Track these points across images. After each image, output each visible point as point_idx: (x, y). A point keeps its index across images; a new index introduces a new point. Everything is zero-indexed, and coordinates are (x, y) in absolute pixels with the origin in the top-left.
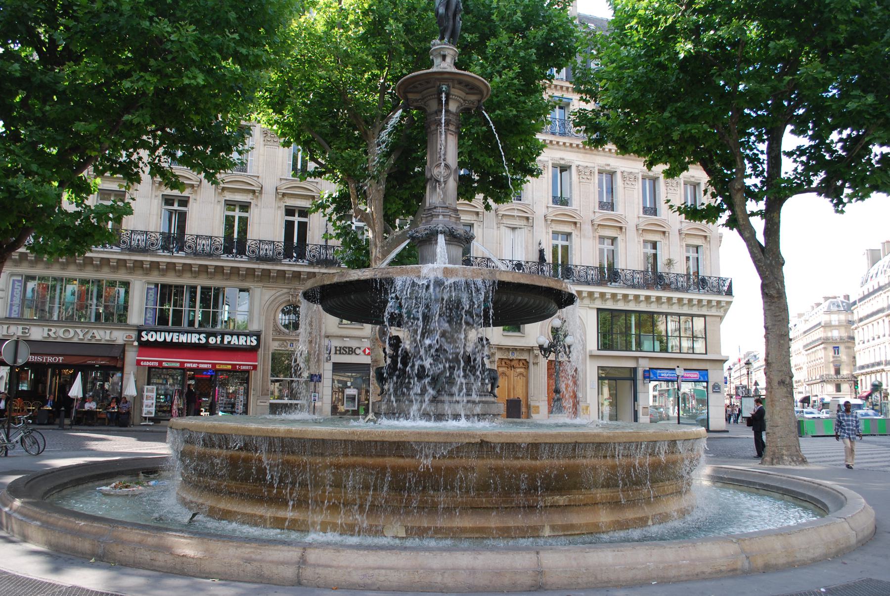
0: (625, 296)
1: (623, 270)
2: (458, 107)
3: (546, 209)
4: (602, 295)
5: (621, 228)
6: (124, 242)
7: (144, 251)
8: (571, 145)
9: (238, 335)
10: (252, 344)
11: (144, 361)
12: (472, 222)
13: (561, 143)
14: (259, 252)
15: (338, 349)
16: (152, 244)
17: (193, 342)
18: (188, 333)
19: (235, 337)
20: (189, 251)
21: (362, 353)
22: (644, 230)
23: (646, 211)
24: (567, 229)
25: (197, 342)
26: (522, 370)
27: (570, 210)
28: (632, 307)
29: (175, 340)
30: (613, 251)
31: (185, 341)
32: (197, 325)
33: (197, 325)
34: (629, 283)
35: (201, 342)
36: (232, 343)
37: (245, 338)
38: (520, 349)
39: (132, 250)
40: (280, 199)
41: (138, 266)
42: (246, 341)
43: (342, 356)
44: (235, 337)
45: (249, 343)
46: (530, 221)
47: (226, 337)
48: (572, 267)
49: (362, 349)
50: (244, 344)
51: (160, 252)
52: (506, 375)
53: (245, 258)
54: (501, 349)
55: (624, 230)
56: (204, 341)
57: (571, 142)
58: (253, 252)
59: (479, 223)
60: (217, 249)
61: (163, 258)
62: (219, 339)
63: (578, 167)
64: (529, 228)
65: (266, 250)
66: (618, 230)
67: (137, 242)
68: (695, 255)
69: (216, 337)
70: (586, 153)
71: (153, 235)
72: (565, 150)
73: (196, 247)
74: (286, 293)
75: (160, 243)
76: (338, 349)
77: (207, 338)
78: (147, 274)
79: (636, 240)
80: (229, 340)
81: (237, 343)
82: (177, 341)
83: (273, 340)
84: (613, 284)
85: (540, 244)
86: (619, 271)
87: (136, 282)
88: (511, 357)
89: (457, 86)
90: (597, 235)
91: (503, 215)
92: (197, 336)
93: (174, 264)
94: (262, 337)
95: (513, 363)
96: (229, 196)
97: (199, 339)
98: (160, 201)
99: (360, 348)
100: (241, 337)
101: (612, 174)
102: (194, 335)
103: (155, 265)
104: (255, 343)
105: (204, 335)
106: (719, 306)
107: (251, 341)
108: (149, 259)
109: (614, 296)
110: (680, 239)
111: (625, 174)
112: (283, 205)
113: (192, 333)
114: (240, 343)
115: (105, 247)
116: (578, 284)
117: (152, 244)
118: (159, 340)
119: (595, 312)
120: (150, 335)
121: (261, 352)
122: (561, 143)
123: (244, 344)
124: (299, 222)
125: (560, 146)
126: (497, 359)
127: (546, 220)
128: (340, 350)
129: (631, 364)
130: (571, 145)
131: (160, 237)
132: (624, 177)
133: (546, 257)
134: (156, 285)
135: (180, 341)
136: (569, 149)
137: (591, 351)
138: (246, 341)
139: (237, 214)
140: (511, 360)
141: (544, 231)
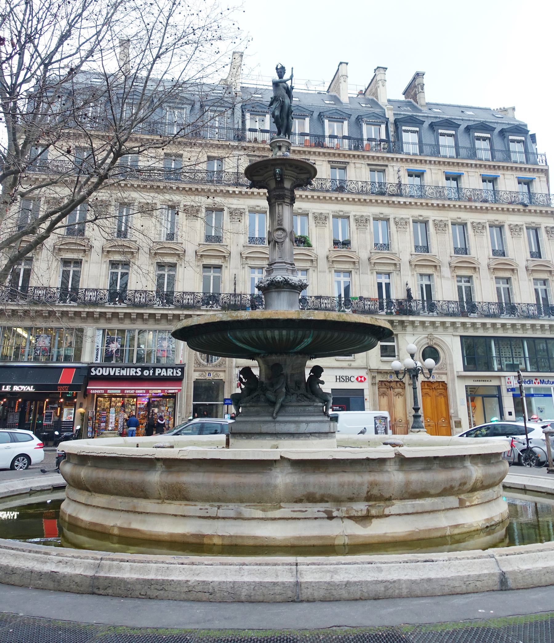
0: (484, 325)
2: (292, 184)
3: (410, 256)
4: (464, 324)
5: (475, 268)
6: (80, 298)
7: (95, 304)
10: (177, 375)
11: (93, 389)
12: (350, 270)
13: (457, 206)
14: (183, 301)
15: (338, 377)
16: (101, 299)
17: (131, 374)
18: (127, 367)
19: (164, 370)
20: (129, 303)
21: (356, 381)
22: (494, 269)
24: (507, 274)
25: (134, 374)
26: (400, 390)
27: (468, 258)
29: (117, 374)
30: (508, 288)
31: (125, 374)
32: (135, 361)
33: (135, 361)
34: (525, 314)
35: (137, 374)
36: (162, 375)
37: (172, 370)
38: (384, 372)
39: (85, 304)
40: (199, 260)
41: (90, 315)
42: (173, 373)
43: (341, 383)
44: (164, 370)
45: (175, 374)
46: (398, 266)
47: (157, 370)
48: (435, 302)
49: (356, 377)
50: (171, 375)
51: (107, 305)
52: (386, 395)
53: (172, 307)
54: (381, 373)
55: (477, 270)
56: (139, 374)
58: (178, 301)
59: (356, 270)
60: (199, 302)
61: (109, 309)
62: (151, 372)
64: (397, 272)
65: (91, 296)
67: (89, 298)
69: (149, 371)
70: (440, 210)
71: (102, 291)
72: (422, 209)
73: (134, 300)
74: (424, 338)
75: (107, 297)
76: (338, 377)
77: (142, 372)
78: (97, 322)
79: (489, 278)
80: (160, 372)
81: (165, 375)
82: (119, 374)
83: (195, 371)
84: (472, 314)
85: (407, 284)
86: (476, 304)
87: (89, 328)
88: (389, 379)
89: (289, 168)
90: (455, 275)
91: (375, 263)
92: (135, 370)
93: (118, 313)
94: (186, 369)
95: (392, 384)
96: (159, 259)
97: (136, 372)
98: (108, 265)
100: (169, 370)
102: (132, 369)
103: (102, 315)
104: (180, 374)
105: (140, 369)
106: (525, 328)
107: (177, 373)
108: (98, 310)
109: (503, 325)
110: (527, 274)
111: (474, 224)
112: (201, 264)
113: (130, 368)
114: (168, 375)
115: (116, 304)
116: (442, 316)
117: (101, 299)
118: (104, 374)
119: (459, 338)
120: (97, 371)
121: (185, 381)
122: (419, 204)
123: (171, 375)
124: (118, 273)
125: (418, 206)
126: (377, 382)
127: (411, 265)
129: (495, 383)
130: (503, 209)
131: (107, 293)
134: (104, 330)
135: (121, 374)
136: (425, 207)
138: (173, 373)
140: (391, 382)
141: (410, 273)
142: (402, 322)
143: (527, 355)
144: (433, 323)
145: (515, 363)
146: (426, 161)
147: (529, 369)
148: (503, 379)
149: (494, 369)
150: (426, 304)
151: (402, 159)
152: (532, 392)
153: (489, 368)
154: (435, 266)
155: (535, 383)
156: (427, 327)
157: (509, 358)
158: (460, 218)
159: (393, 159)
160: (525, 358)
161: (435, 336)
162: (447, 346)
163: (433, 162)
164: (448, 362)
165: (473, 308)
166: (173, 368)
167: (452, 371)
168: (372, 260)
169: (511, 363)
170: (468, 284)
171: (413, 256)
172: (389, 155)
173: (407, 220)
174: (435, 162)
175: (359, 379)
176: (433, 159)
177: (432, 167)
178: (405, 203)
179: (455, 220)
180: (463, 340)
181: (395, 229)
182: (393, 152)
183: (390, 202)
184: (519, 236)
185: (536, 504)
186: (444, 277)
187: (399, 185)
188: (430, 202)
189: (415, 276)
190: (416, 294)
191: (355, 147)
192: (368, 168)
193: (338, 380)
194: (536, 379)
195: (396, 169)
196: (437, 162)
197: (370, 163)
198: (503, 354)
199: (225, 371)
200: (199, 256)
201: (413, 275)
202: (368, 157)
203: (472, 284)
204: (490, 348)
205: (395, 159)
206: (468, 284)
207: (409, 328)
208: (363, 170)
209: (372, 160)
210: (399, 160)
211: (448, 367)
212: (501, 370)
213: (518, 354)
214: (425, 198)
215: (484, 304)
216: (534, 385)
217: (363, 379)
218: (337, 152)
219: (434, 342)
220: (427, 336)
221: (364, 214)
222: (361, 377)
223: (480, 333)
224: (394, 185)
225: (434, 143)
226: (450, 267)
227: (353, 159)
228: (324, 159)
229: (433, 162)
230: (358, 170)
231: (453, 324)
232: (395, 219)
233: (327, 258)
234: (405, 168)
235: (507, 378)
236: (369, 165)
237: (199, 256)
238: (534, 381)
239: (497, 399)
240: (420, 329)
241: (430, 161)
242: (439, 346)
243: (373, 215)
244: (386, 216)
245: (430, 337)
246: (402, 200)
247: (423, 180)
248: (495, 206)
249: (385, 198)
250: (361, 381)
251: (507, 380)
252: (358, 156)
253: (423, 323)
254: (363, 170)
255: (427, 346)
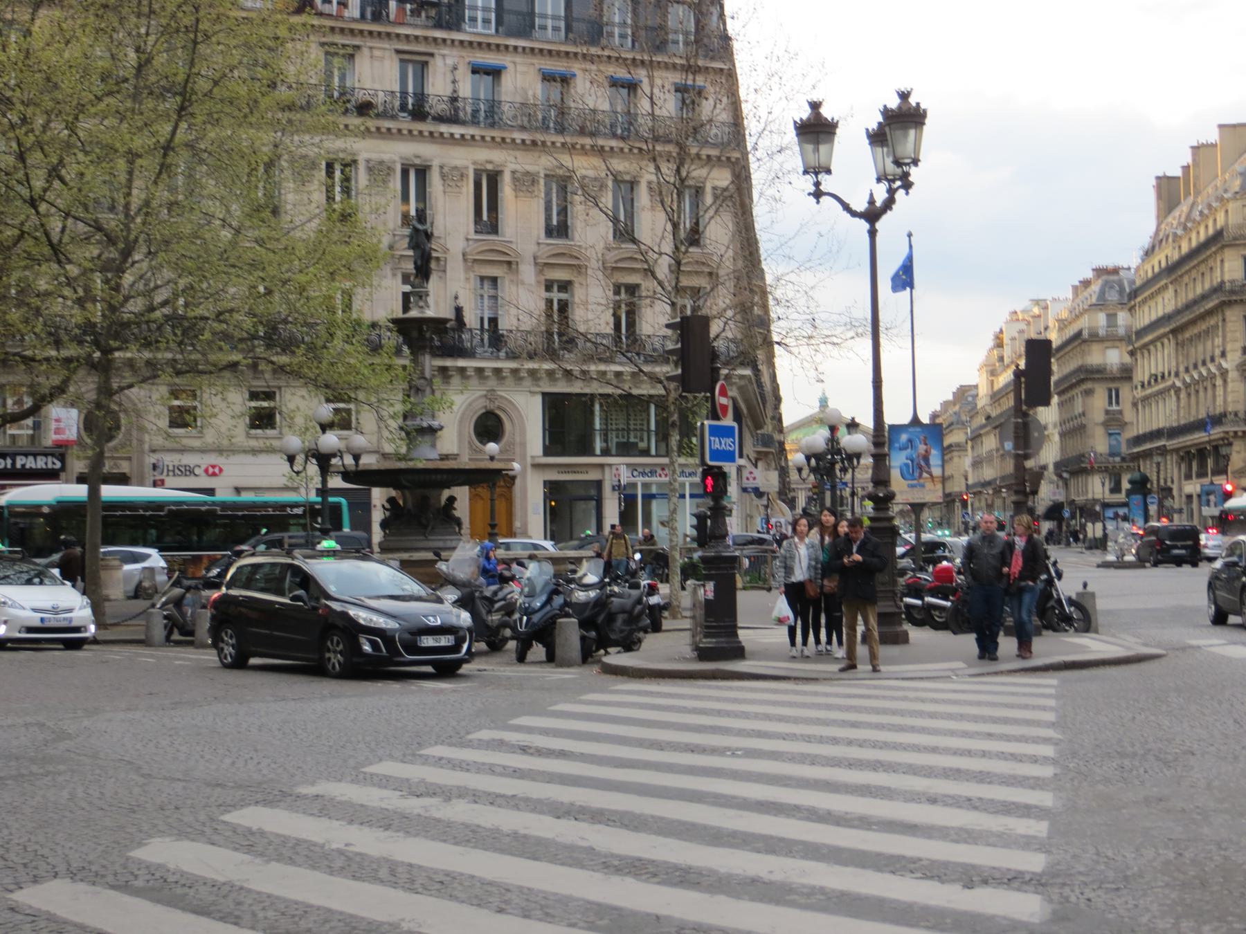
1: (649, 336)
8: (483, 138)
9: (35, 455)
10: (55, 467)
21: (203, 474)
23: (549, 232)
28: (595, 388)
37: (44, 458)
42: (46, 464)
46: (442, 263)
49: (203, 467)
57: (483, 134)
62: (9, 461)
63: (513, 172)
64: (440, 274)
66: (505, 266)
68: (492, 292)
74: (481, 397)
81: (34, 467)
90: (543, 278)
99: (199, 466)
101: (494, 178)
107: (54, 463)
111: (446, 170)
114: (39, 467)
119: (539, 399)
123: (44, 467)
124: (560, 301)
127: (465, 260)
128: (174, 471)
129: (593, 476)
132: (443, 176)
133: (466, 320)
137: (533, 457)
138: (46, 464)
139: (556, 296)
141: (462, 276)
142: (443, 370)
143: (653, 427)
144: (497, 371)
145: (632, 440)
146: (507, 47)
147: (653, 452)
148: (607, 470)
149: (593, 449)
150: (486, 336)
151: (462, 42)
152: (654, 490)
153: (587, 450)
154: (509, 263)
155: (660, 476)
156: (486, 378)
157: (642, 430)
158: (490, 162)
159: (444, 40)
160: (649, 431)
161: (499, 393)
162: (519, 412)
163: (520, 50)
164: (518, 439)
165: (569, 342)
166: (46, 455)
167: (524, 456)
168: (397, 250)
169: (625, 440)
170: (563, 296)
171: (471, 242)
172: (439, 34)
173: (465, 172)
174: (524, 48)
175: (211, 470)
176: (521, 43)
177: (518, 59)
178: (462, 136)
179: (481, 165)
180: (547, 398)
181: (441, 188)
182: (449, 27)
183: (436, 135)
184: (458, 189)
185: (875, 670)
186: (523, 283)
187: (454, 99)
188: (508, 136)
189: (472, 281)
190: (471, 319)
191: (373, 14)
192: (396, 58)
193: (171, 473)
194: (663, 469)
195: (450, 61)
196: (527, 50)
197: (324, 40)
198: (614, 422)
199: (129, 459)
200: (542, 267)
201: (467, 279)
202: (398, 35)
203: (572, 295)
204: (592, 413)
205: (449, 42)
206: (563, 296)
207: (456, 380)
208: (387, 63)
209: (433, 45)
210: (456, 43)
211: (518, 449)
212: (606, 452)
213: (639, 422)
214: (500, 128)
215: (656, 339)
216: (659, 478)
217: (217, 470)
218: (339, 24)
219: (497, 403)
220: (484, 393)
221: (385, 157)
222: (213, 467)
223: (577, 388)
224: (445, 99)
225: (525, 10)
226: (536, 264)
227: (368, 39)
228: (387, 46)
229: (520, 50)
230: (376, 64)
231: (533, 373)
232: (441, 167)
233: (535, 258)
234: (468, 60)
235: (614, 467)
236: (398, 52)
237: (611, 270)
238: (659, 471)
239: (594, 502)
240: (474, 382)
241: (516, 48)
242: (504, 411)
243: (401, 158)
244: (426, 161)
245: (490, 395)
246: (457, 130)
247: (499, 84)
248: (489, 134)
249: (426, 127)
250: (214, 474)
251: (614, 471)
252: (379, 34)
253: (480, 371)
254: (387, 63)
255: (484, 411)
